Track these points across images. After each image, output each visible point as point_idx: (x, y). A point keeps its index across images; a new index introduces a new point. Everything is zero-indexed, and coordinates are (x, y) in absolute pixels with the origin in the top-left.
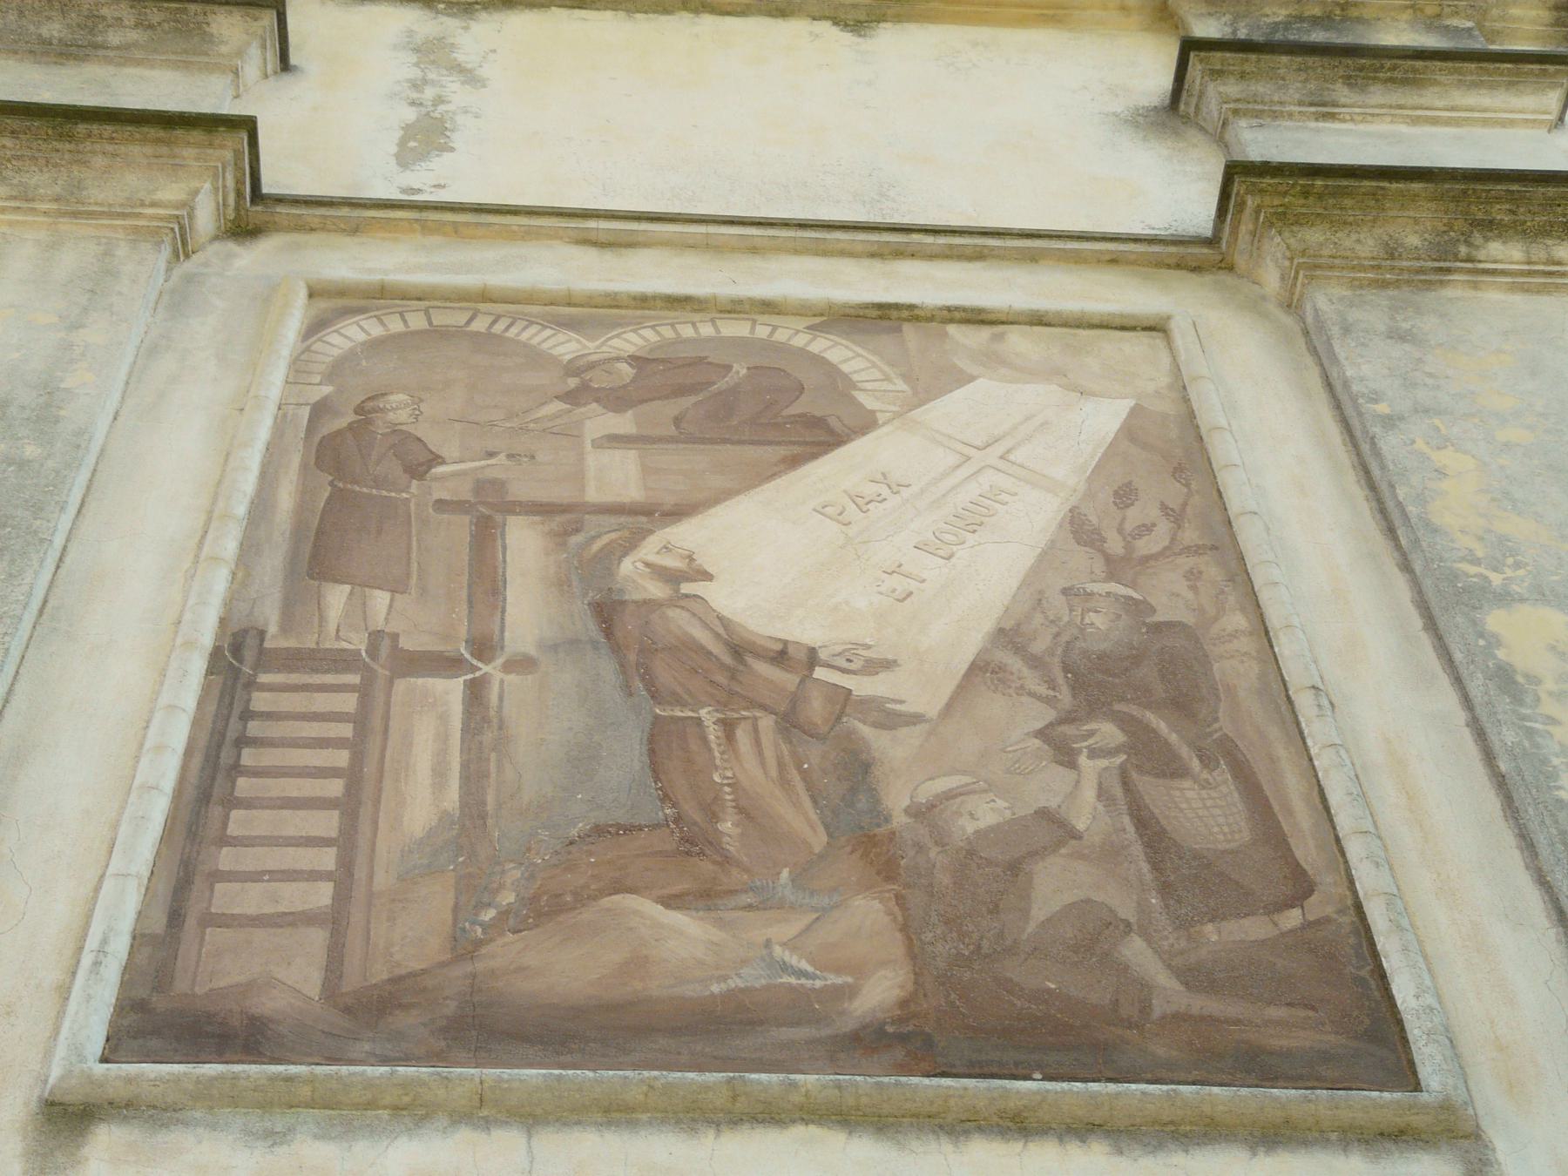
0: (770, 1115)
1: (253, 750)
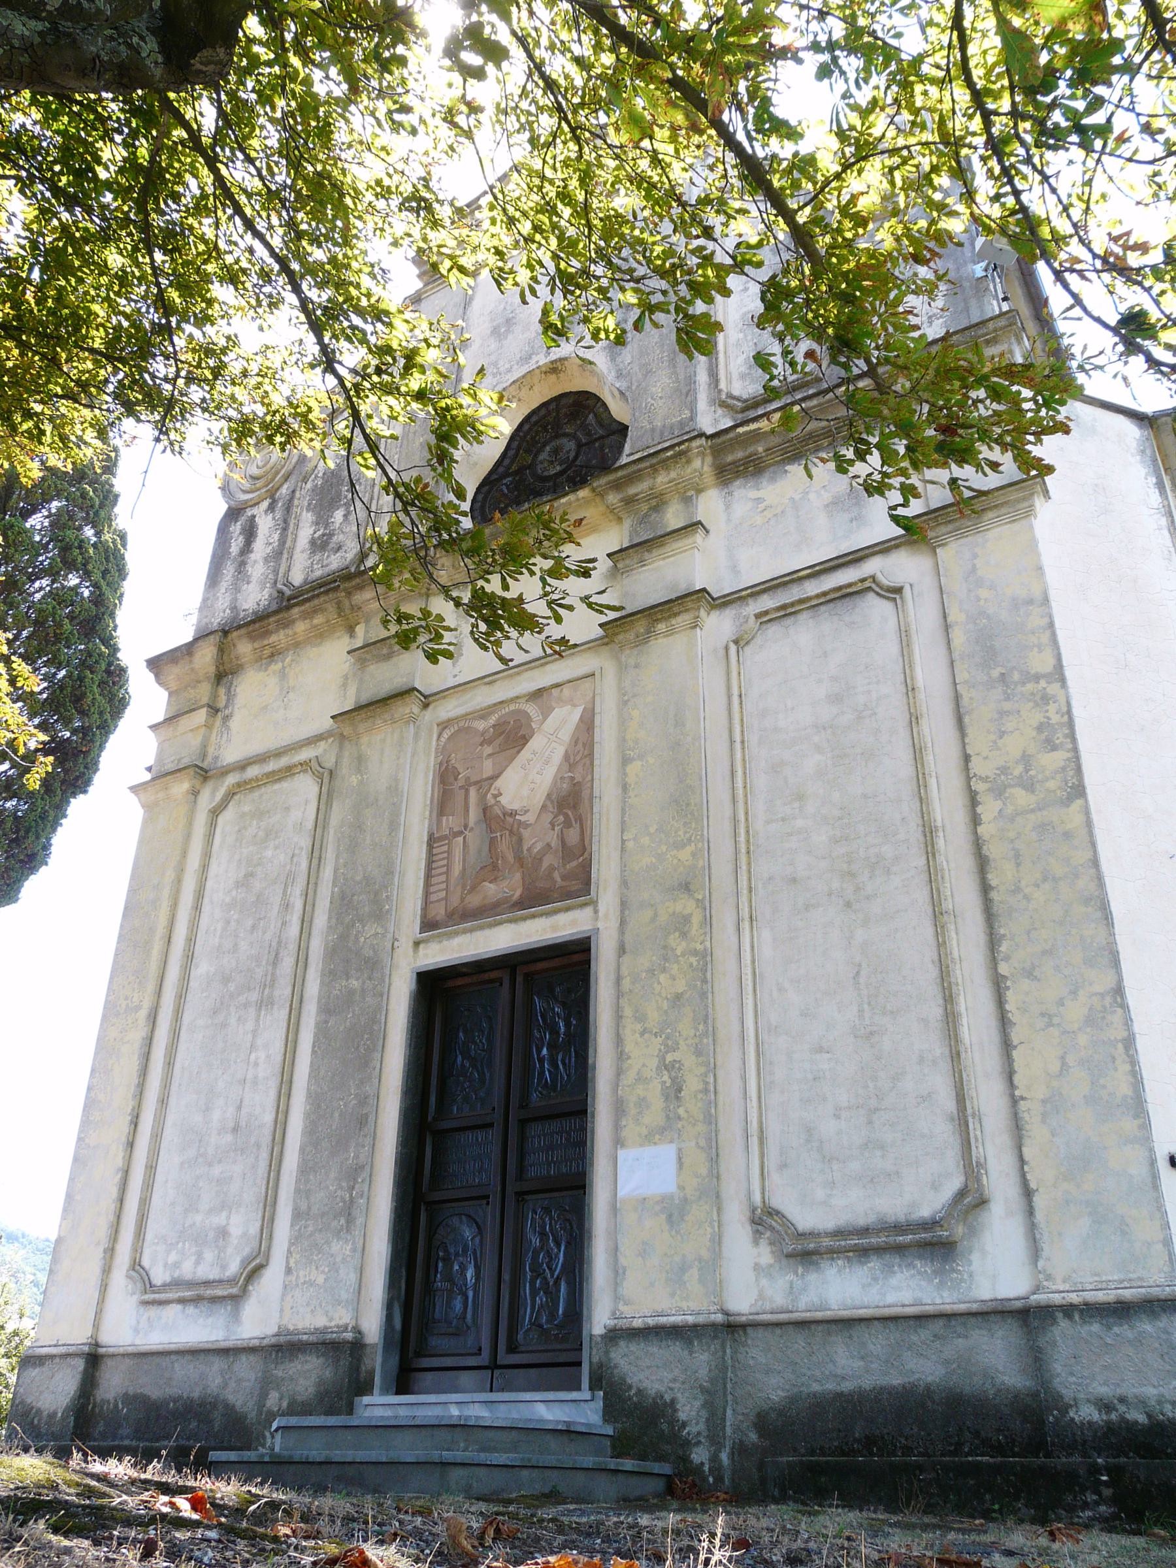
0: (500, 923)
1: (81, 1368)
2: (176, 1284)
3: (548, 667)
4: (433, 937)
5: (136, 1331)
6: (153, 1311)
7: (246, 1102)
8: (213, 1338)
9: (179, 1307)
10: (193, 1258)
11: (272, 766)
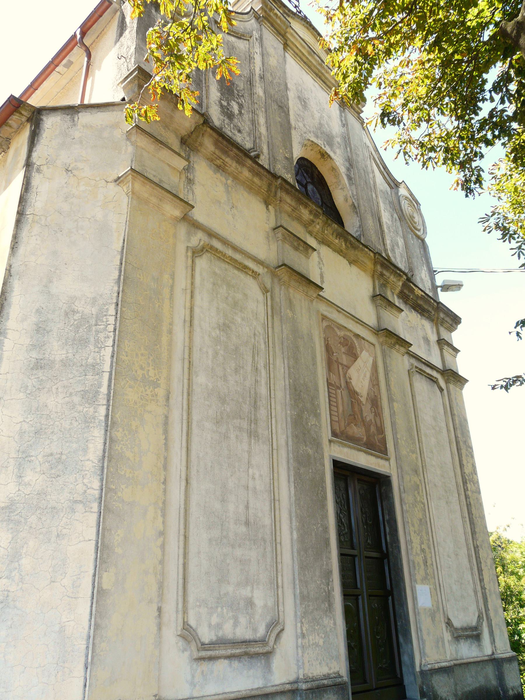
2: (221, 642)
3: (358, 325)
4: (338, 442)
5: (193, 684)
6: (205, 666)
7: (251, 505)
8: (256, 686)
9: (226, 662)
10: (232, 622)
11: (238, 257)
